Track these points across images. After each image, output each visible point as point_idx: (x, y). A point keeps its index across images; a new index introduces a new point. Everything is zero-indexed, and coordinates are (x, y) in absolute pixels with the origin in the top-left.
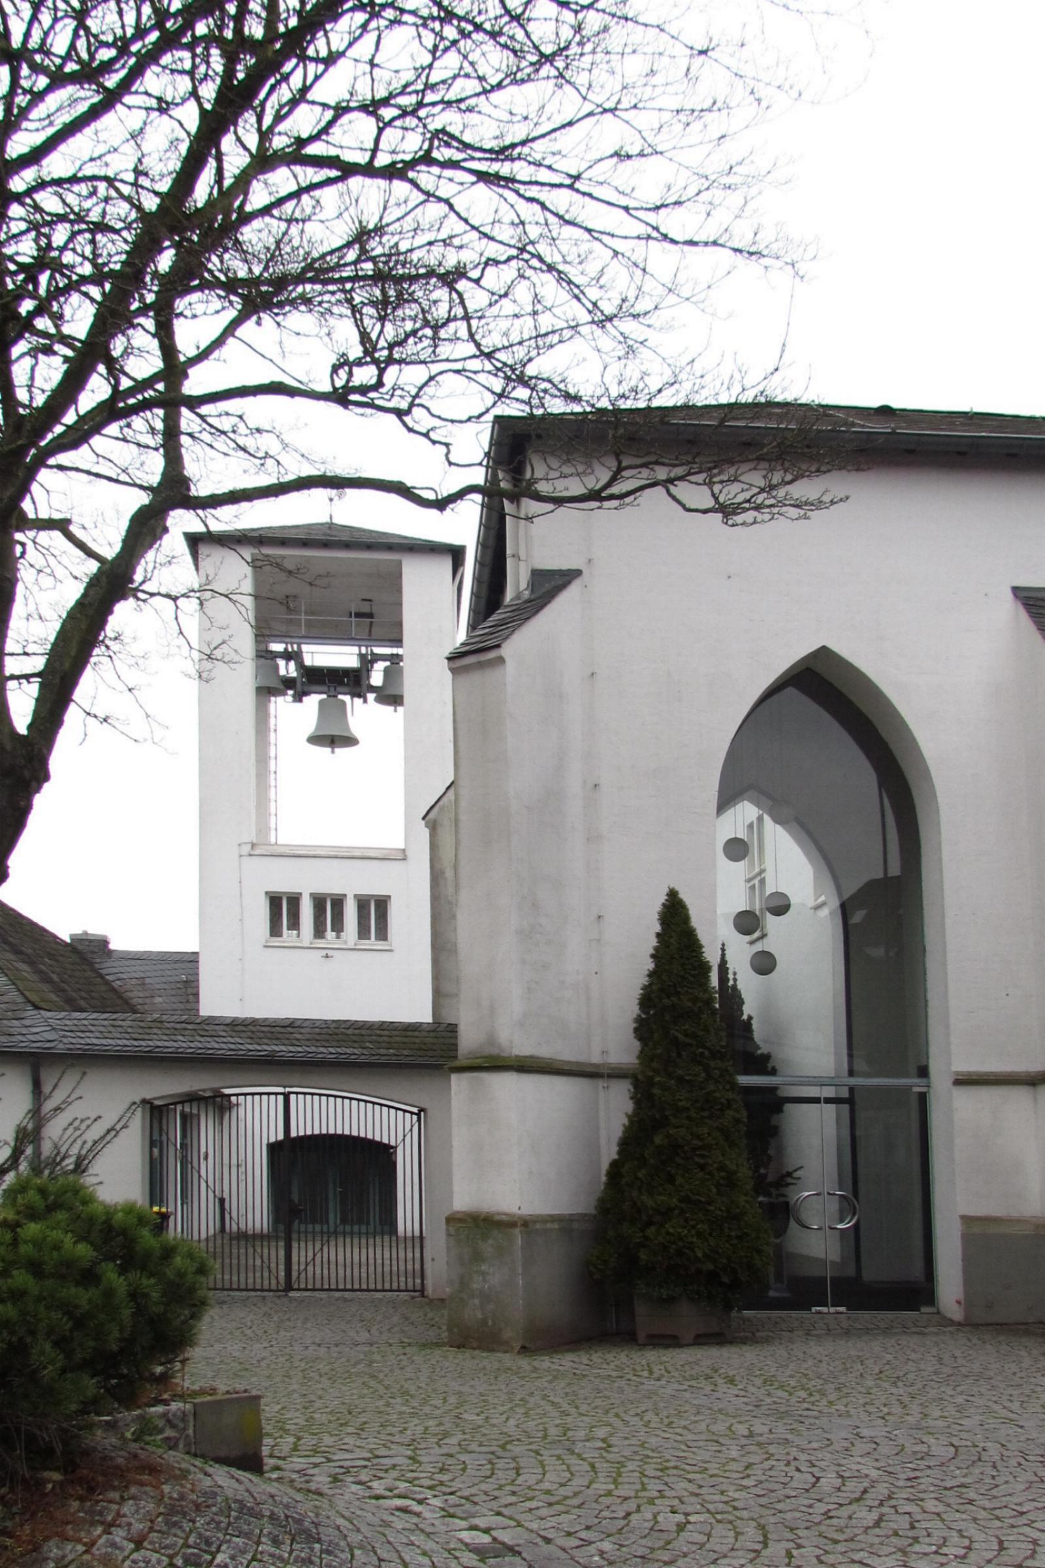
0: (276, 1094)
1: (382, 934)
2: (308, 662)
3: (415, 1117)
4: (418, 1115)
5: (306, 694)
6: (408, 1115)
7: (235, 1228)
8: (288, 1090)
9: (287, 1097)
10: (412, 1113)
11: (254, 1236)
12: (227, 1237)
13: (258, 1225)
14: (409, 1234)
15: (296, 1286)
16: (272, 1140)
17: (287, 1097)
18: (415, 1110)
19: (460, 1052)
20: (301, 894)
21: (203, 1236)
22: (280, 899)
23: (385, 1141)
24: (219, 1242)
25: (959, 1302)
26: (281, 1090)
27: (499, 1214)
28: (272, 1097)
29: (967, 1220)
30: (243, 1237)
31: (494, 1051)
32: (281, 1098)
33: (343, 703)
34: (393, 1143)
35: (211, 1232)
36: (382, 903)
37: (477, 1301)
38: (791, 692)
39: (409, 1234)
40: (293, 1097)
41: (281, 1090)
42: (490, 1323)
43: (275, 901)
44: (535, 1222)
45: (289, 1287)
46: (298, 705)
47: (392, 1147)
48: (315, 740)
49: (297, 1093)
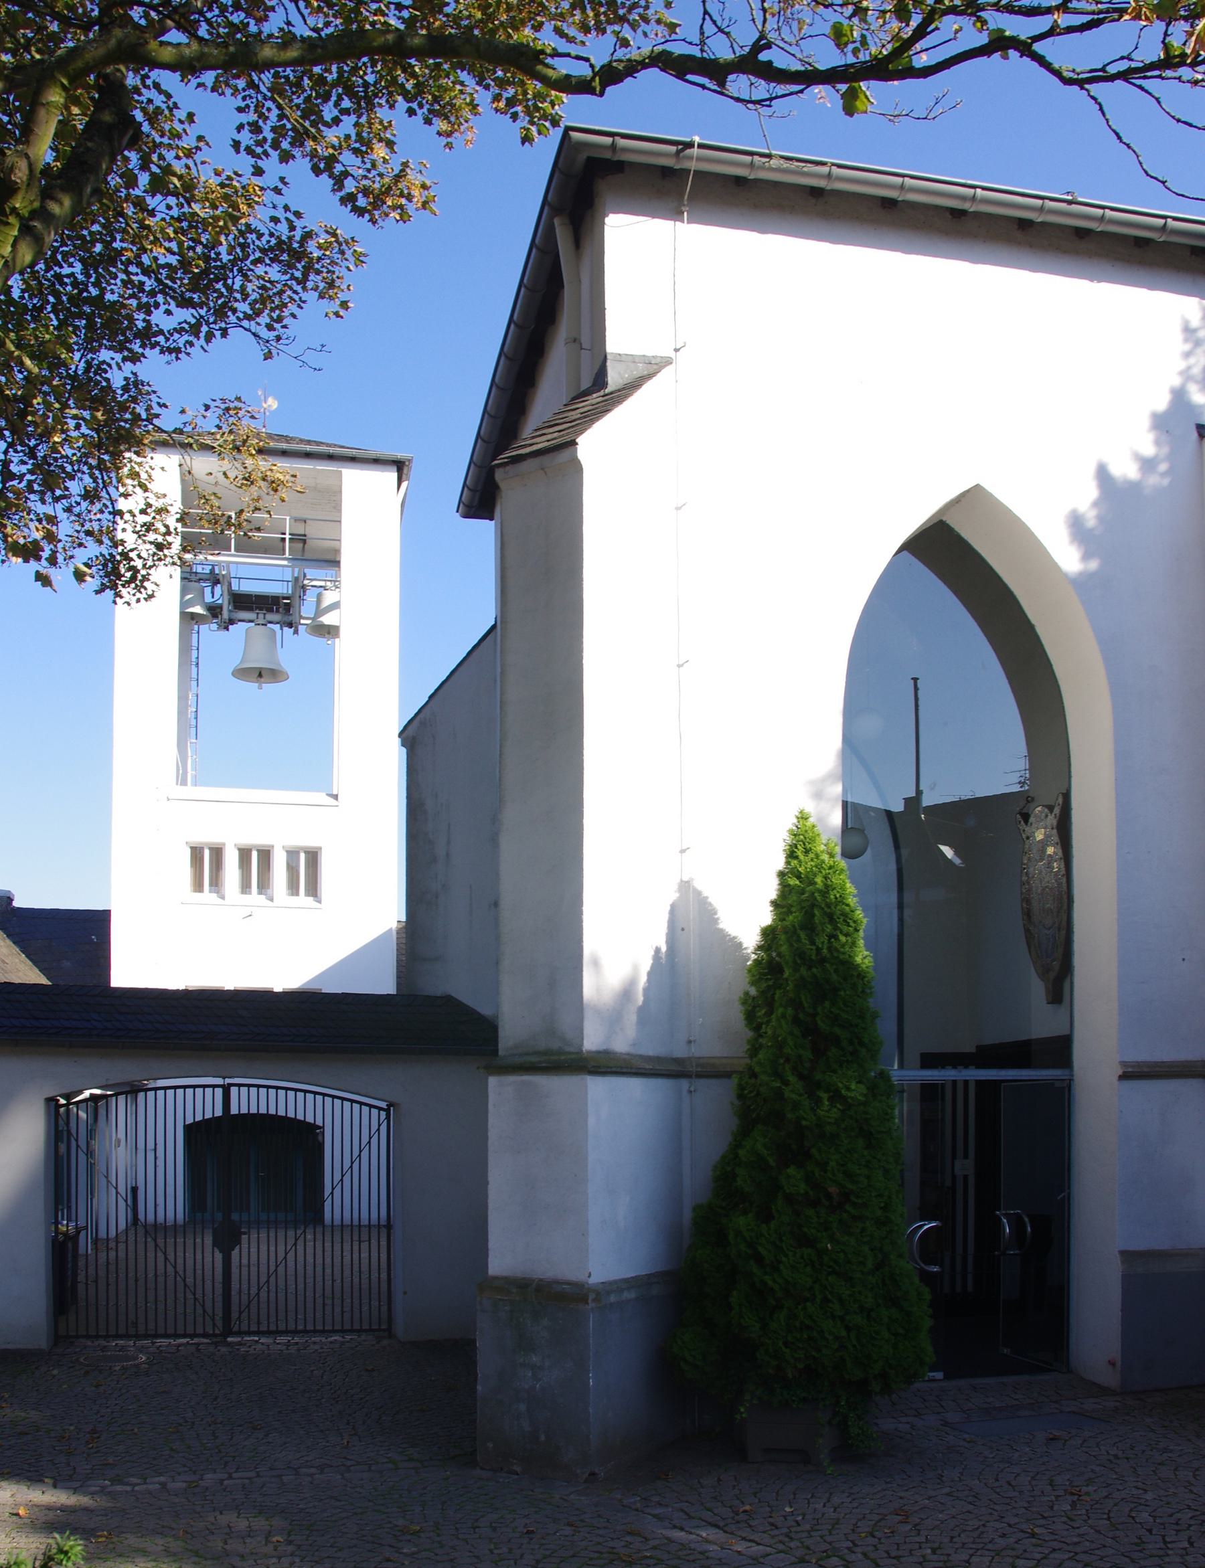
0: (214, 1086)
1: (313, 889)
2: (235, 587)
3: (383, 1114)
4: (388, 1111)
5: (232, 622)
6: (375, 1112)
7: (151, 1217)
8: (228, 1081)
9: (226, 1089)
10: (380, 1109)
11: (165, 1227)
12: (141, 1230)
13: (170, 1214)
14: (337, 1221)
15: (235, 1329)
16: (190, 1121)
17: (226, 1089)
18: (383, 1105)
19: (501, 1046)
20: (224, 844)
21: (113, 1234)
22: (201, 849)
23: (310, 1119)
24: (131, 1238)
25: (1112, 1363)
26: (219, 1081)
27: (557, 1282)
28: (209, 1091)
29: (1128, 1256)
30: (157, 1230)
31: (555, 1045)
32: (219, 1091)
33: (274, 631)
34: (319, 1122)
35: (122, 1226)
36: (313, 857)
37: (523, 1407)
38: (905, 553)
39: (337, 1221)
40: (234, 1090)
41: (219, 1081)
42: (543, 1438)
43: (196, 853)
44: (608, 1293)
45: (228, 1332)
46: (224, 633)
47: (319, 1127)
48: (242, 673)
49: (239, 1085)
